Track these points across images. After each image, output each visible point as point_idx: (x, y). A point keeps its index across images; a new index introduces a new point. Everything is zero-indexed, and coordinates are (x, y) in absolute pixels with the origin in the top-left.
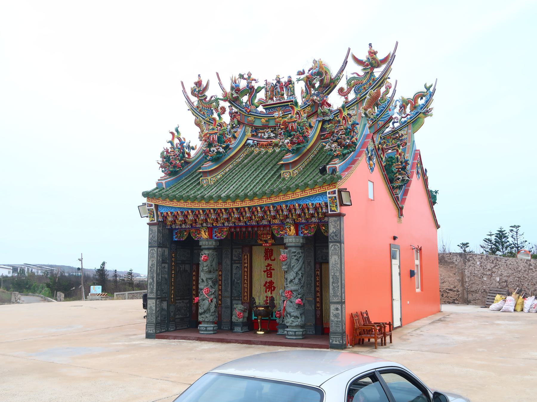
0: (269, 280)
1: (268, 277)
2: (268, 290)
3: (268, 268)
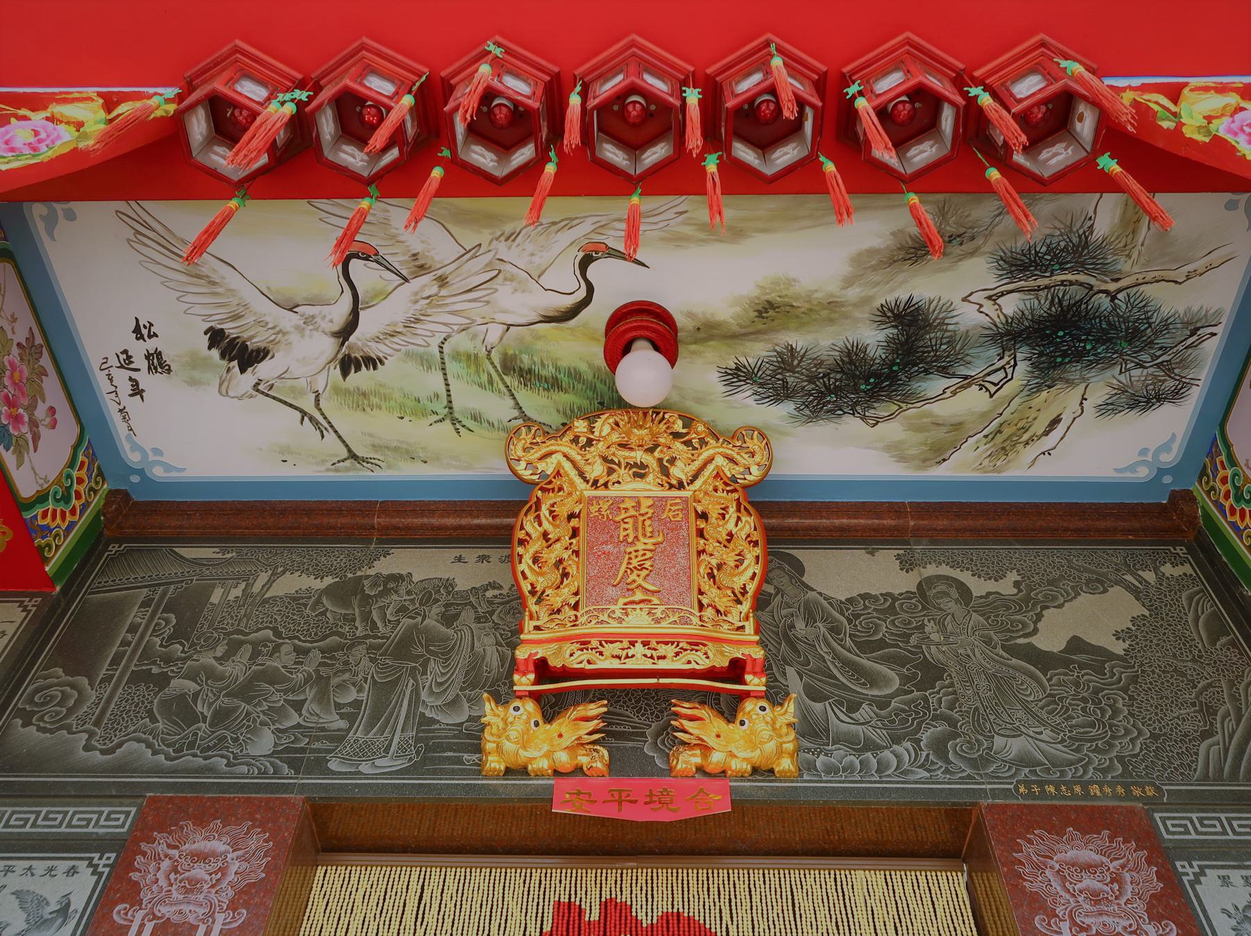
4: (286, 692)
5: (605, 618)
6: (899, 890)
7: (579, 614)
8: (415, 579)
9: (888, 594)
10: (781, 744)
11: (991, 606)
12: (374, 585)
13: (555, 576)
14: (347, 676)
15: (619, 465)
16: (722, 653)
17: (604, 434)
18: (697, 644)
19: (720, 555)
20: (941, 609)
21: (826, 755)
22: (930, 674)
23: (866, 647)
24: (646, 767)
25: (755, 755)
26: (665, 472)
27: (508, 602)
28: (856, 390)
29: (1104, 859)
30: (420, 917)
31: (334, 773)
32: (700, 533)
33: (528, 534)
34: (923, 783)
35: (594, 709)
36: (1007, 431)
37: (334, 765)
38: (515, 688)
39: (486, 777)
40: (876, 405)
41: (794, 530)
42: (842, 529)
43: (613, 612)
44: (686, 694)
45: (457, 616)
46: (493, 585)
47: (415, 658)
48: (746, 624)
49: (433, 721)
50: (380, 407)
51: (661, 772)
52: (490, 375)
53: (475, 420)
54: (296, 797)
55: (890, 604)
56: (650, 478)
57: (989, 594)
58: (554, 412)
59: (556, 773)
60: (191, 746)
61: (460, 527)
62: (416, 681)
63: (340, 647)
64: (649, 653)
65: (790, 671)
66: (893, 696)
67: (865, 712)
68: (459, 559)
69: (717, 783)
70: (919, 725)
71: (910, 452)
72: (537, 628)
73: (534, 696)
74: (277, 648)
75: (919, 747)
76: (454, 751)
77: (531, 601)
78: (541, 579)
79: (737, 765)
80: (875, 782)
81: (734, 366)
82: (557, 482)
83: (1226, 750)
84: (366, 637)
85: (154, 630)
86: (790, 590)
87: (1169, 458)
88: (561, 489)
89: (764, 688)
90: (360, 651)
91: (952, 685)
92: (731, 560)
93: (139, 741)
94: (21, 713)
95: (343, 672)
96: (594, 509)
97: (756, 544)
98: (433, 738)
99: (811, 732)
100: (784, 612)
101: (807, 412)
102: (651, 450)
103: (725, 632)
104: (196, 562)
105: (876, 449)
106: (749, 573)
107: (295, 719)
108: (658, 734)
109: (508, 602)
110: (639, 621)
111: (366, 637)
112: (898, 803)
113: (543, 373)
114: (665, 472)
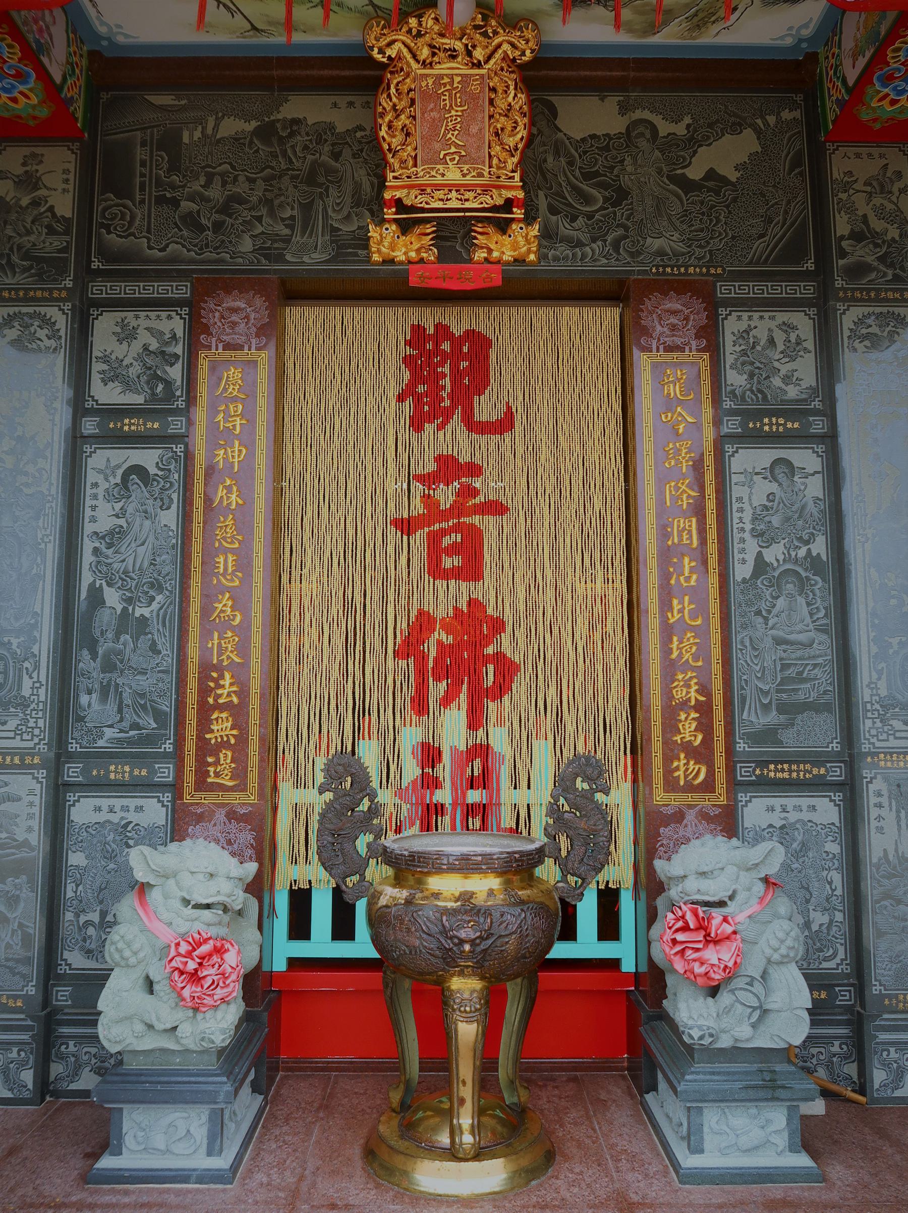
0: (445, 598)
1: (436, 571)
2: (437, 689)
3: (446, 495)
4: (250, 209)
5: (433, 173)
6: (585, 317)
9: (607, 135)
11: (672, 141)
14: (282, 198)
15: (439, 49)
20: (637, 147)
22: (620, 196)
23: (587, 176)
24: (457, 258)
27: (371, 142)
29: (684, 309)
30: (344, 332)
31: (289, 262)
32: (491, 102)
33: (384, 108)
36: (701, 15)
37: (288, 257)
44: (479, 219)
46: (361, 128)
47: (320, 185)
48: (515, 174)
49: (339, 230)
53: (339, 6)
56: (459, 59)
57: (669, 134)
60: (207, 246)
65: (541, 194)
66: (597, 211)
67: (580, 221)
68: (335, 105)
69: (494, 266)
72: (395, 178)
73: (395, 220)
74: (236, 179)
78: (394, 140)
79: (505, 258)
83: (768, 246)
84: (288, 169)
85: (157, 166)
87: (806, 33)
88: (402, 69)
89: (411, 660)
90: (286, 180)
91: (632, 203)
93: (177, 243)
94: (102, 225)
95: (280, 195)
99: (547, 235)
100: (541, 149)
103: (503, 181)
104: (162, 108)
106: (519, 136)
107: (259, 229)
109: (371, 142)
110: (453, 175)
111: (288, 169)
114: (469, 54)
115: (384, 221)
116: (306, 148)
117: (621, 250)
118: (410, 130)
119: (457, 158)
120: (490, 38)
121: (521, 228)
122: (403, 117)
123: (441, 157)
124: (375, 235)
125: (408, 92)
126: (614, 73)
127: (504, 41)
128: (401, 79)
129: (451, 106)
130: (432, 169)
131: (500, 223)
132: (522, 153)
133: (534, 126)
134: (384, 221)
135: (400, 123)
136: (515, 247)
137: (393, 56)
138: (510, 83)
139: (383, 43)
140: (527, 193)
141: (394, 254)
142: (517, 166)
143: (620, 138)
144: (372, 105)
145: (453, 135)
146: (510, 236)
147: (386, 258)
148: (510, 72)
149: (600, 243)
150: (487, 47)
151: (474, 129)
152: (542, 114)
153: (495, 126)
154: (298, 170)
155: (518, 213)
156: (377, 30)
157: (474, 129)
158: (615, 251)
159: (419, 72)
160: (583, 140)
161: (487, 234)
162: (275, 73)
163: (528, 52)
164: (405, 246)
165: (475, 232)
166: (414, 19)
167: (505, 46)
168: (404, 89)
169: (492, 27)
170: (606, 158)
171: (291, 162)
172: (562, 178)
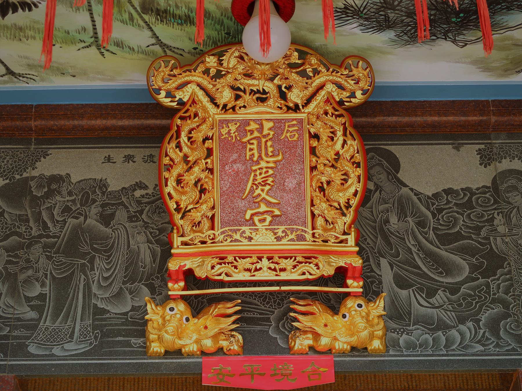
5: (237, 236)
7: (217, 234)
8: (74, 180)
9: (468, 189)
10: (373, 332)
12: (40, 186)
13: (195, 194)
14: (30, 272)
15: (244, 91)
16: (329, 264)
17: (231, 66)
18: (310, 258)
19: (328, 174)
20: (509, 203)
21: (407, 334)
23: (445, 239)
24: (271, 347)
25: (354, 340)
26: (283, 96)
28: (448, 22)
32: (313, 151)
33: (171, 160)
34: (478, 355)
35: (231, 308)
37: (32, 349)
38: (170, 293)
39: (151, 357)
40: (465, 32)
41: (393, 127)
42: (433, 126)
43: (244, 232)
45: (113, 215)
46: (140, 186)
47: (83, 255)
49: (104, 311)
50: (34, 38)
51: (283, 351)
52: (131, 15)
53: (118, 45)
54: (9, 376)
55: (467, 200)
56: (271, 102)
58: (186, 40)
59: (203, 353)
61: (107, 128)
62: (86, 276)
63: (21, 246)
64: (272, 266)
65: (384, 262)
67: (440, 297)
68: (108, 159)
69: (323, 358)
70: (481, 307)
71: (494, 65)
73: (183, 297)
75: (479, 326)
76: (124, 336)
77: (177, 217)
78: (184, 198)
79: (339, 346)
80: (443, 355)
81: (343, 6)
82: (193, 109)
84: (40, 236)
86: (388, 186)
88: (196, 115)
90: (37, 250)
91: (509, 272)
92: (337, 178)
95: (27, 268)
96: (224, 131)
97: (358, 165)
98: (106, 325)
99: (397, 315)
100: (381, 208)
101: (406, 38)
102: (272, 80)
103: (332, 246)
105: (465, 63)
106: (352, 190)
108: (280, 319)
109: (153, 202)
110: (263, 239)
112: (458, 371)
113: (178, 12)
114: (283, 96)
115: (169, 298)
116: (66, 210)
117: (501, 333)
118: (205, 186)
119: (269, 219)
120: (309, 78)
121: (360, 306)
122: (196, 169)
123: (248, 217)
124: (154, 317)
125: (204, 141)
126: (470, 118)
127: (327, 81)
128: (194, 125)
129: (260, 157)
130: (236, 231)
131: (330, 300)
132: (356, 211)
133: (370, 180)
134: (169, 298)
135: (192, 177)
136: (352, 331)
137: (185, 100)
138: (337, 128)
139: (172, 84)
140: (366, 260)
141: (181, 342)
142: (350, 227)
143: (485, 193)
144: (156, 159)
145: (263, 190)
146: (344, 316)
147: (170, 348)
148: (337, 116)
149: (470, 324)
150: (306, 88)
151: (291, 183)
152: (379, 163)
153: (319, 179)
154: (54, 237)
155: (354, 286)
156: (165, 71)
157: (291, 183)
158: (493, 335)
159: (218, 117)
160: (436, 196)
161: (312, 314)
162: (33, 123)
163: (359, 94)
164: (198, 332)
165: (295, 311)
166: (212, 57)
167: (330, 87)
168: (199, 136)
169: (311, 65)
170: (469, 216)
171: (45, 227)
172: (411, 243)
